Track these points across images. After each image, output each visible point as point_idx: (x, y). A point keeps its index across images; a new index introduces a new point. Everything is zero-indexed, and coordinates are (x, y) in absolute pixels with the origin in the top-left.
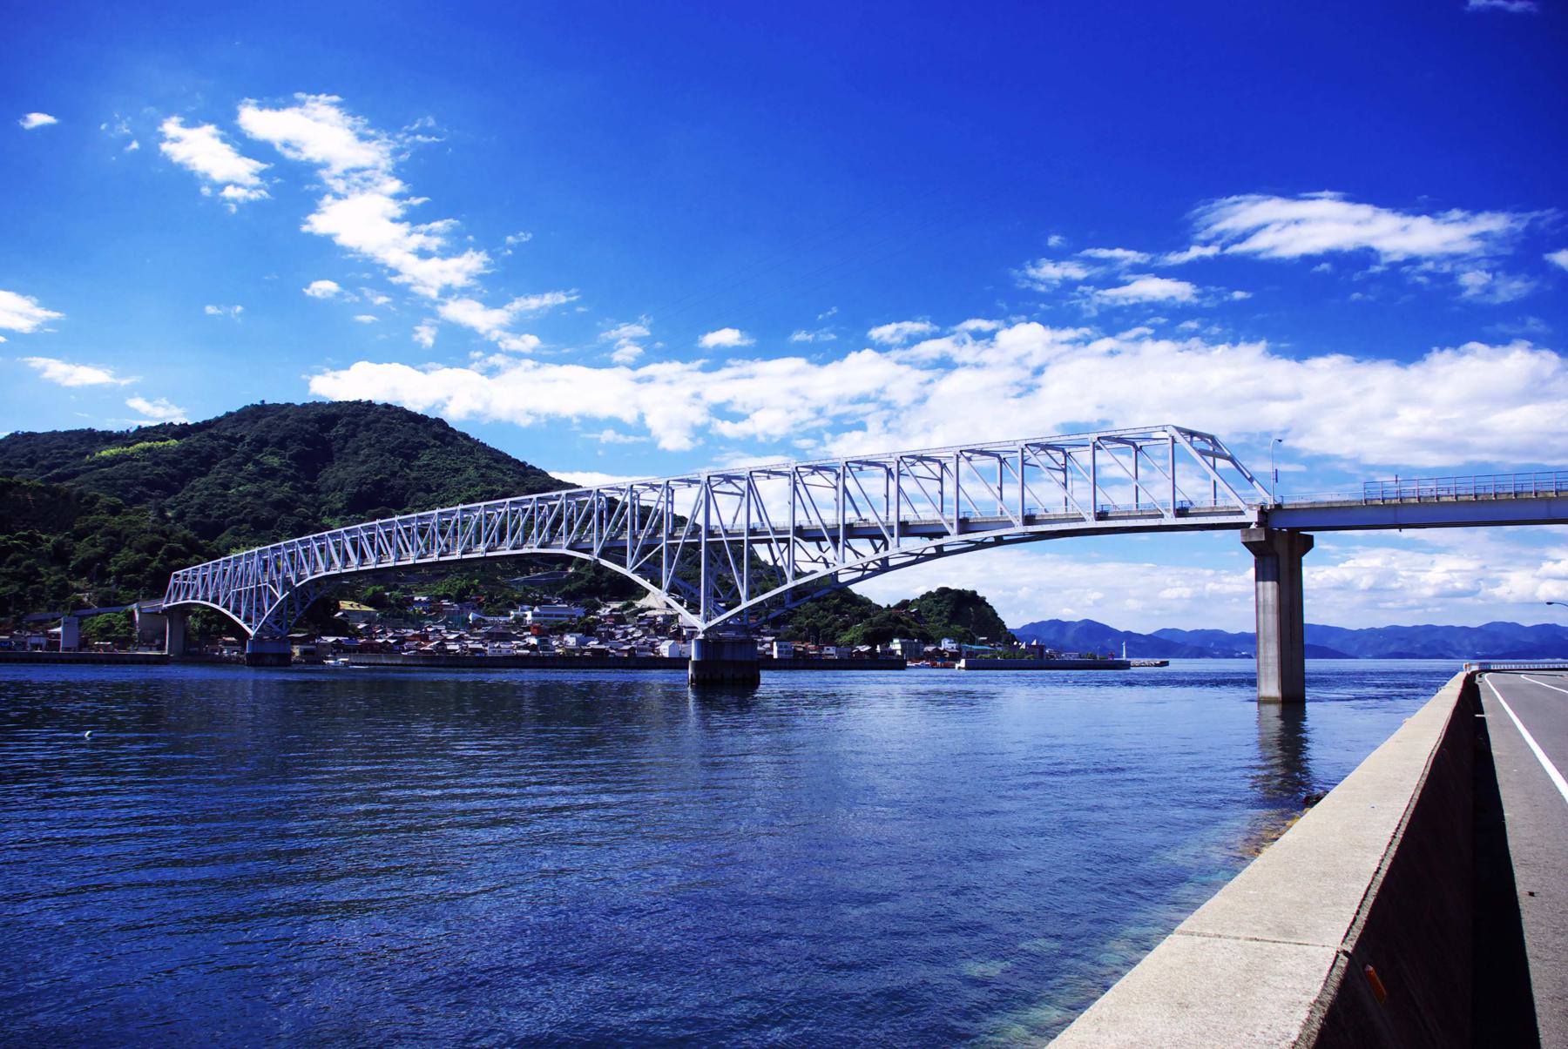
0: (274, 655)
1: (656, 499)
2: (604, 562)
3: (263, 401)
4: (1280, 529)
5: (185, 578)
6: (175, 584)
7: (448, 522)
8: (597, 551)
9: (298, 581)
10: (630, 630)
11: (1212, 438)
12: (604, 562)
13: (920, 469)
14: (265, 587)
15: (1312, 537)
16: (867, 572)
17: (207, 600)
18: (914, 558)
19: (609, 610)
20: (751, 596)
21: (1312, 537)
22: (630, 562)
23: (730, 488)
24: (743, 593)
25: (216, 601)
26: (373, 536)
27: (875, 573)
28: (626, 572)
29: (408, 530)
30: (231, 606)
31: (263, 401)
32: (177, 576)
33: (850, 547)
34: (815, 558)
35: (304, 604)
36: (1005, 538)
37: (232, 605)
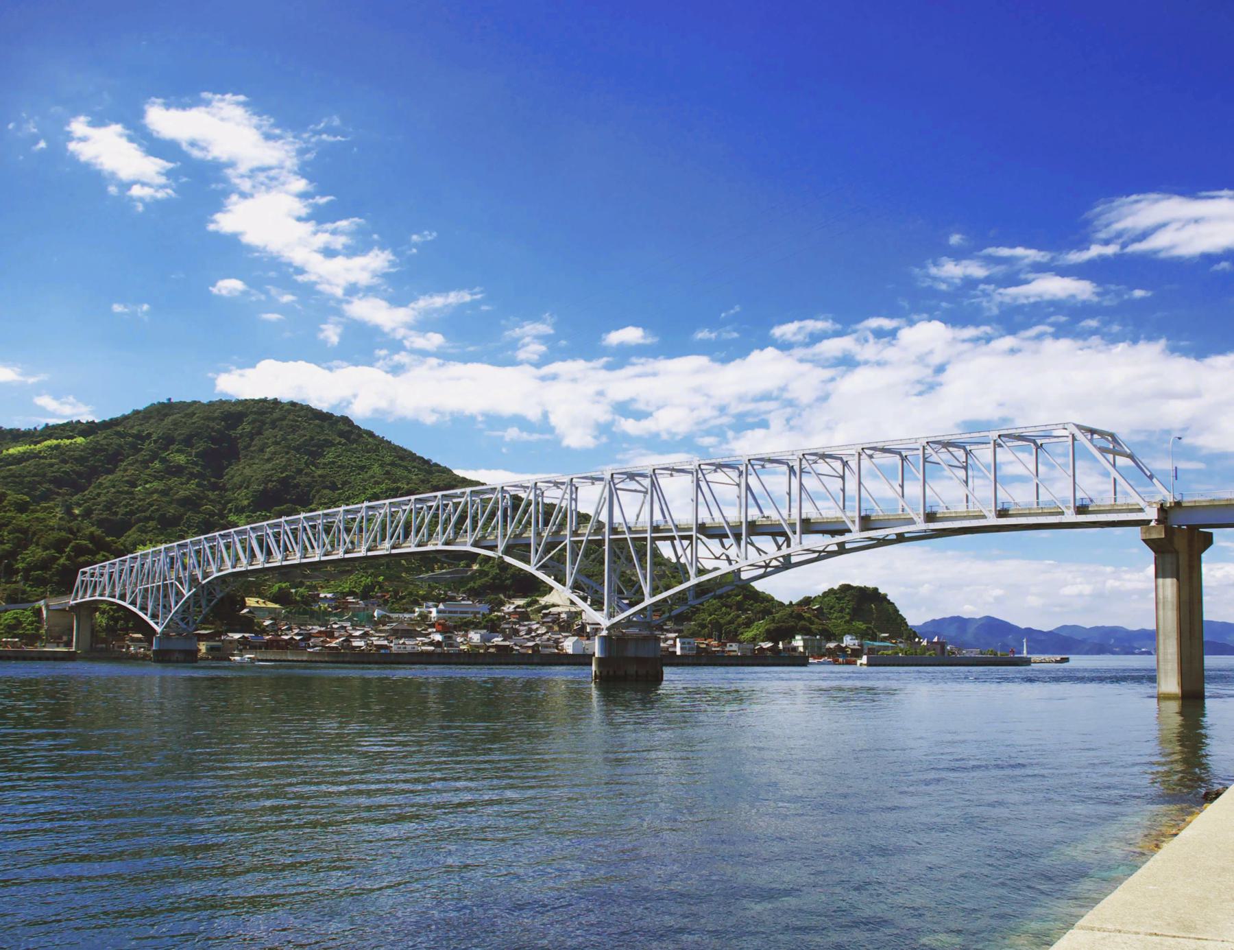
0: (180, 651)
1: (560, 496)
2: (508, 559)
3: (170, 399)
4: (1180, 526)
5: (92, 575)
6: (83, 581)
7: (354, 520)
8: (501, 548)
9: (204, 578)
10: (534, 627)
11: (1112, 435)
12: (508, 559)
13: (822, 467)
14: (172, 583)
15: (1211, 534)
16: (769, 569)
17: (114, 597)
18: (816, 555)
19: (513, 606)
20: (655, 591)
21: (1211, 534)
22: (534, 559)
23: (633, 485)
24: (646, 590)
25: (123, 597)
26: (279, 533)
27: (778, 570)
28: (530, 569)
29: (313, 527)
30: (138, 603)
31: (170, 399)
32: (84, 573)
33: (752, 544)
34: (718, 556)
35: (210, 601)
36: (906, 535)
37: (139, 601)
